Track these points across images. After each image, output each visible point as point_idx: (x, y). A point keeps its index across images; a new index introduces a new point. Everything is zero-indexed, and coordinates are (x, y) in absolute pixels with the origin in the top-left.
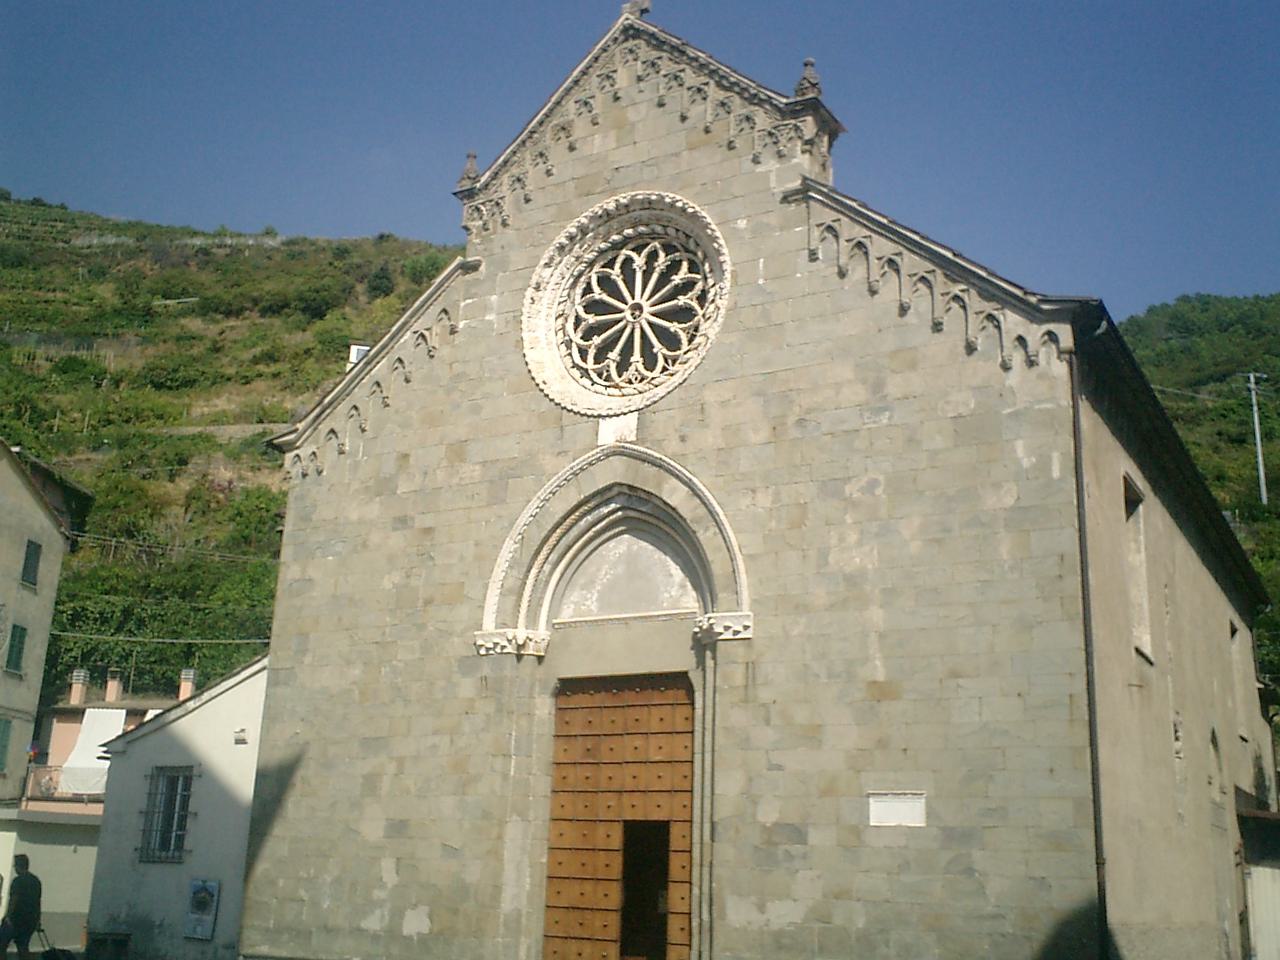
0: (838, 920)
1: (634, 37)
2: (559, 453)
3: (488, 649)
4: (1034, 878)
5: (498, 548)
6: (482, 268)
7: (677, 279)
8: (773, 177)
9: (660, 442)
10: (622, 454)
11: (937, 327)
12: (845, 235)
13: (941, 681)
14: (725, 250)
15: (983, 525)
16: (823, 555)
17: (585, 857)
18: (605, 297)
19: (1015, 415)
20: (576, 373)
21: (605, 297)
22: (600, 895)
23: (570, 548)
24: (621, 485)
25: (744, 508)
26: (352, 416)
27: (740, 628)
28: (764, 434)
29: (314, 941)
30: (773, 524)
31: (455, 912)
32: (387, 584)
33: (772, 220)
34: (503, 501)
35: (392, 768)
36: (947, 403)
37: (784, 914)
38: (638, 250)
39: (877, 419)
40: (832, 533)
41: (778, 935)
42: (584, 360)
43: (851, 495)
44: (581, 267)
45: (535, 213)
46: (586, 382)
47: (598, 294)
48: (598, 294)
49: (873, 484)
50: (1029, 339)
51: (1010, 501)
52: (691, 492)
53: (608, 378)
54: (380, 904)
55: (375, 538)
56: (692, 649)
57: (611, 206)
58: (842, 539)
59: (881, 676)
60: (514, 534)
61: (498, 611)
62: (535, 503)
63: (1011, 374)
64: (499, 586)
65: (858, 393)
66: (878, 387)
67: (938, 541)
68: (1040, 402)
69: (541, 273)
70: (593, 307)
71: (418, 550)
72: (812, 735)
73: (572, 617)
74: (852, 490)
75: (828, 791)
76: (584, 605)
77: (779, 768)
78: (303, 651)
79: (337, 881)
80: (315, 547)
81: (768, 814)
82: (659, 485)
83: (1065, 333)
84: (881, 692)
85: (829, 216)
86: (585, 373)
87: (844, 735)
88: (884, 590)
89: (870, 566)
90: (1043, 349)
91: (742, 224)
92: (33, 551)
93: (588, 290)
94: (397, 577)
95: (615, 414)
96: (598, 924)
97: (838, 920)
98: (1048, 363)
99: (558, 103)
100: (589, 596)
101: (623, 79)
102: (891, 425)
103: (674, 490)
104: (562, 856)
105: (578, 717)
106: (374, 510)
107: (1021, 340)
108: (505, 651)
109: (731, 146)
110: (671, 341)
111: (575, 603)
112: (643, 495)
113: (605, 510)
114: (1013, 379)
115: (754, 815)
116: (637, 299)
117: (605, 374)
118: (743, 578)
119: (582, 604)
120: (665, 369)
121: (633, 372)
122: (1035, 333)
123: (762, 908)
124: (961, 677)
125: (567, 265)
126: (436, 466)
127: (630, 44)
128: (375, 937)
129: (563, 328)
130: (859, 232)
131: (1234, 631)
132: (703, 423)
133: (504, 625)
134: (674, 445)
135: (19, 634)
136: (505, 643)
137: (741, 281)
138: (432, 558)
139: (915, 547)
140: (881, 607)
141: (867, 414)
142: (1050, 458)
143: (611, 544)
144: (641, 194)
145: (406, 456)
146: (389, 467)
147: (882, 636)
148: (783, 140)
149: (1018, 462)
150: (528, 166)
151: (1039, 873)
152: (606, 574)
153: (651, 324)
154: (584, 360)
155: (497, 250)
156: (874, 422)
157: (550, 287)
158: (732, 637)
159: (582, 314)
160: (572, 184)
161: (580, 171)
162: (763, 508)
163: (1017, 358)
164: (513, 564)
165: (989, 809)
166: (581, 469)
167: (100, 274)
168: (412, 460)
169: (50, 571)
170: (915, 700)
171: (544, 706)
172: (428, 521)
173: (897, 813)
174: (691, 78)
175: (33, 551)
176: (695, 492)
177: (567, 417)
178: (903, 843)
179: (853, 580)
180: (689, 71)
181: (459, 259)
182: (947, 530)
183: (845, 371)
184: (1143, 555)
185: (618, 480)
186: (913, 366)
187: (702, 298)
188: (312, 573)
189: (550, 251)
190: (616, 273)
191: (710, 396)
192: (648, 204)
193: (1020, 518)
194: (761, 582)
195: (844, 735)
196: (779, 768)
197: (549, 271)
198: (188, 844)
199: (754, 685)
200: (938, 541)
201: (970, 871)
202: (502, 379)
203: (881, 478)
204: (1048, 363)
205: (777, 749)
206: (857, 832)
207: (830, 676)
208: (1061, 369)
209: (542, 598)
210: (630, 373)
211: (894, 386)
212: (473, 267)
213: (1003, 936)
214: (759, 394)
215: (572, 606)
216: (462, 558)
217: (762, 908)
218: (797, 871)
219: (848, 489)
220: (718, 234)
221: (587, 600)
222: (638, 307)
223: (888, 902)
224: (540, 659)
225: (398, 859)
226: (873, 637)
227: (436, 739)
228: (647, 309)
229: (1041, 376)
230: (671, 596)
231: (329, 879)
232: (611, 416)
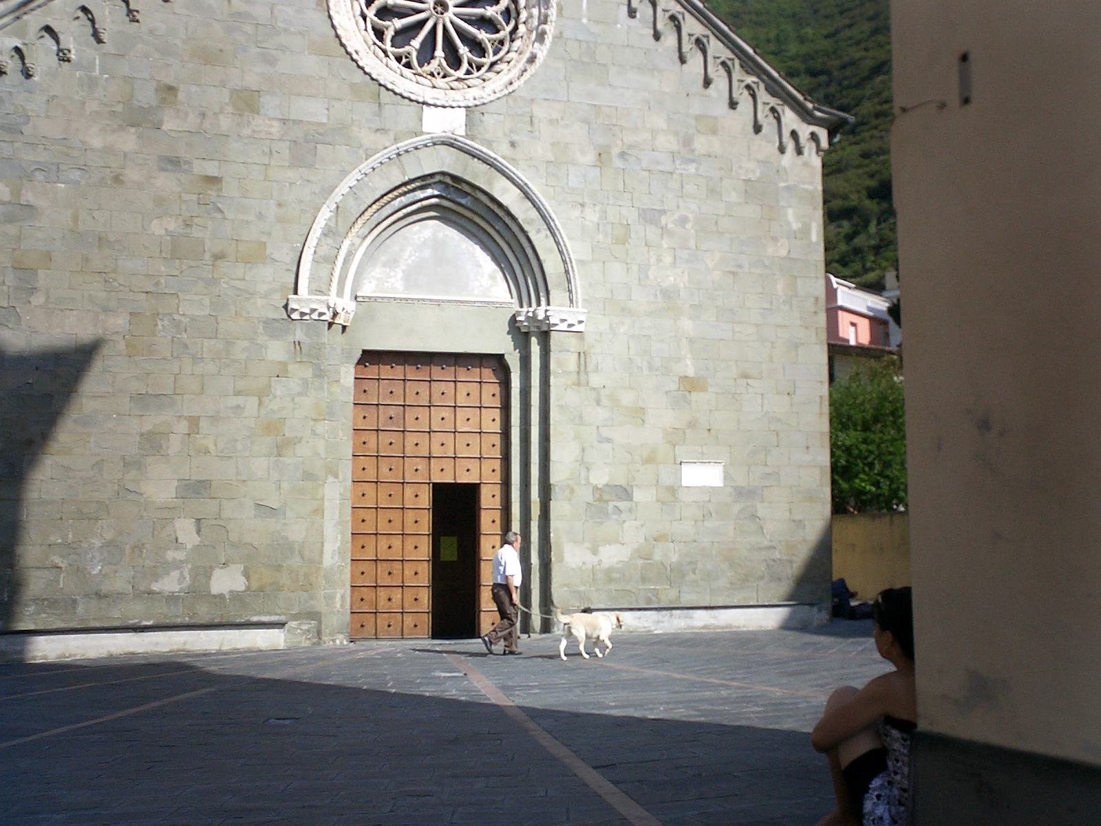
0: (657, 557)
2: (378, 130)
3: (303, 314)
4: (794, 521)
10: (451, 145)
13: (735, 379)
15: (766, 266)
19: (788, 188)
25: (573, 218)
26: (78, 18)
27: (575, 322)
28: (590, 158)
29: (80, 609)
31: (278, 568)
35: (183, 427)
36: (740, 167)
37: (612, 555)
39: (686, 168)
40: (651, 253)
41: (609, 572)
43: (666, 224)
49: (683, 221)
50: (800, 134)
51: (783, 253)
52: (522, 195)
54: (177, 565)
55: (133, 174)
56: (508, 333)
58: (659, 260)
59: (691, 372)
64: (313, 252)
66: (687, 142)
67: (734, 274)
71: (199, 198)
72: (638, 414)
73: (375, 292)
75: (650, 460)
76: (387, 282)
77: (609, 440)
80: (32, 168)
81: (600, 477)
82: (490, 183)
84: (691, 385)
87: (662, 417)
89: (682, 285)
97: (657, 557)
98: (810, 155)
100: (392, 274)
102: (698, 175)
103: (505, 190)
105: (371, 386)
107: (794, 134)
108: (323, 318)
111: (378, 279)
112: (466, 188)
113: (420, 194)
115: (587, 478)
117: (404, 60)
121: (436, 66)
122: (805, 130)
123: (595, 552)
124: (750, 378)
126: (217, 110)
128: (172, 598)
134: (505, 148)
136: (324, 310)
137: (565, 13)
138: (220, 211)
139: (717, 275)
140: (691, 318)
143: (416, 227)
147: (691, 341)
149: (789, 224)
151: (797, 517)
152: (410, 257)
156: (684, 169)
158: (317, 318)
162: (591, 221)
163: (790, 146)
165: (766, 474)
166: (407, 151)
170: (717, 393)
171: (348, 374)
172: (211, 169)
173: (703, 476)
177: (386, 96)
179: (668, 294)
185: (445, 169)
186: (714, 132)
191: (539, 112)
194: (590, 285)
195: (662, 417)
196: (609, 440)
199: (586, 373)
200: (734, 274)
201: (754, 517)
203: (691, 216)
204: (810, 155)
205: (606, 426)
207: (651, 369)
208: (817, 162)
211: (701, 144)
213: (774, 560)
215: (374, 282)
216: (260, 216)
217: (595, 552)
218: (624, 522)
219: (664, 220)
221: (391, 277)
223: (695, 541)
224: (344, 327)
225: (198, 520)
226: (684, 342)
227: (240, 400)
230: (481, 286)
231: (97, 543)
232: (436, 106)
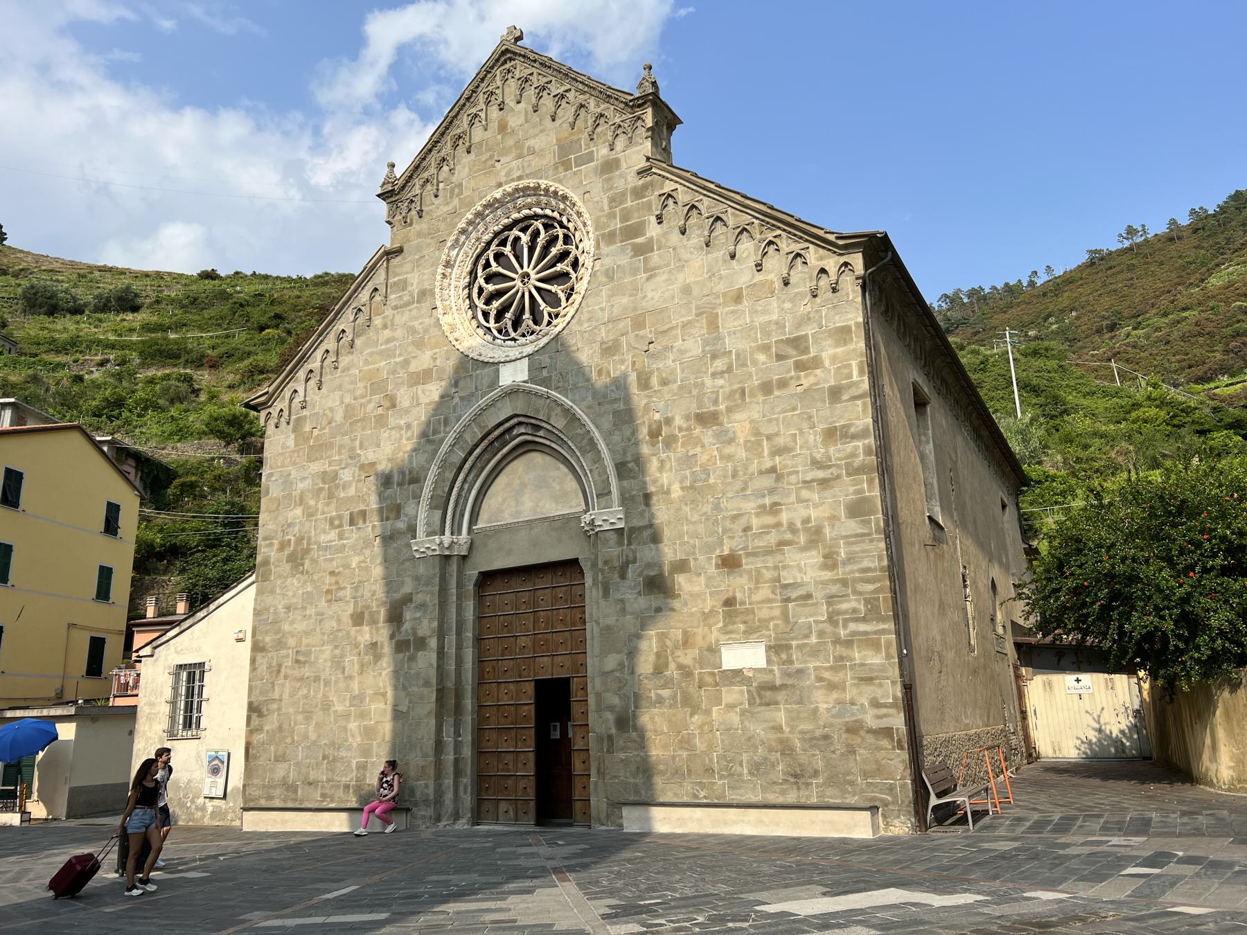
38: (524, 230)
42: (487, 321)
46: (489, 337)
99: (456, 116)
110: (553, 301)
116: (529, 271)
120: (549, 323)
122: (832, 263)
125: (469, 250)
129: (469, 297)
135: (105, 574)
153: (538, 289)
154: (487, 321)
190: (507, 250)
220: (583, 210)
224: (464, 557)
228: (533, 276)
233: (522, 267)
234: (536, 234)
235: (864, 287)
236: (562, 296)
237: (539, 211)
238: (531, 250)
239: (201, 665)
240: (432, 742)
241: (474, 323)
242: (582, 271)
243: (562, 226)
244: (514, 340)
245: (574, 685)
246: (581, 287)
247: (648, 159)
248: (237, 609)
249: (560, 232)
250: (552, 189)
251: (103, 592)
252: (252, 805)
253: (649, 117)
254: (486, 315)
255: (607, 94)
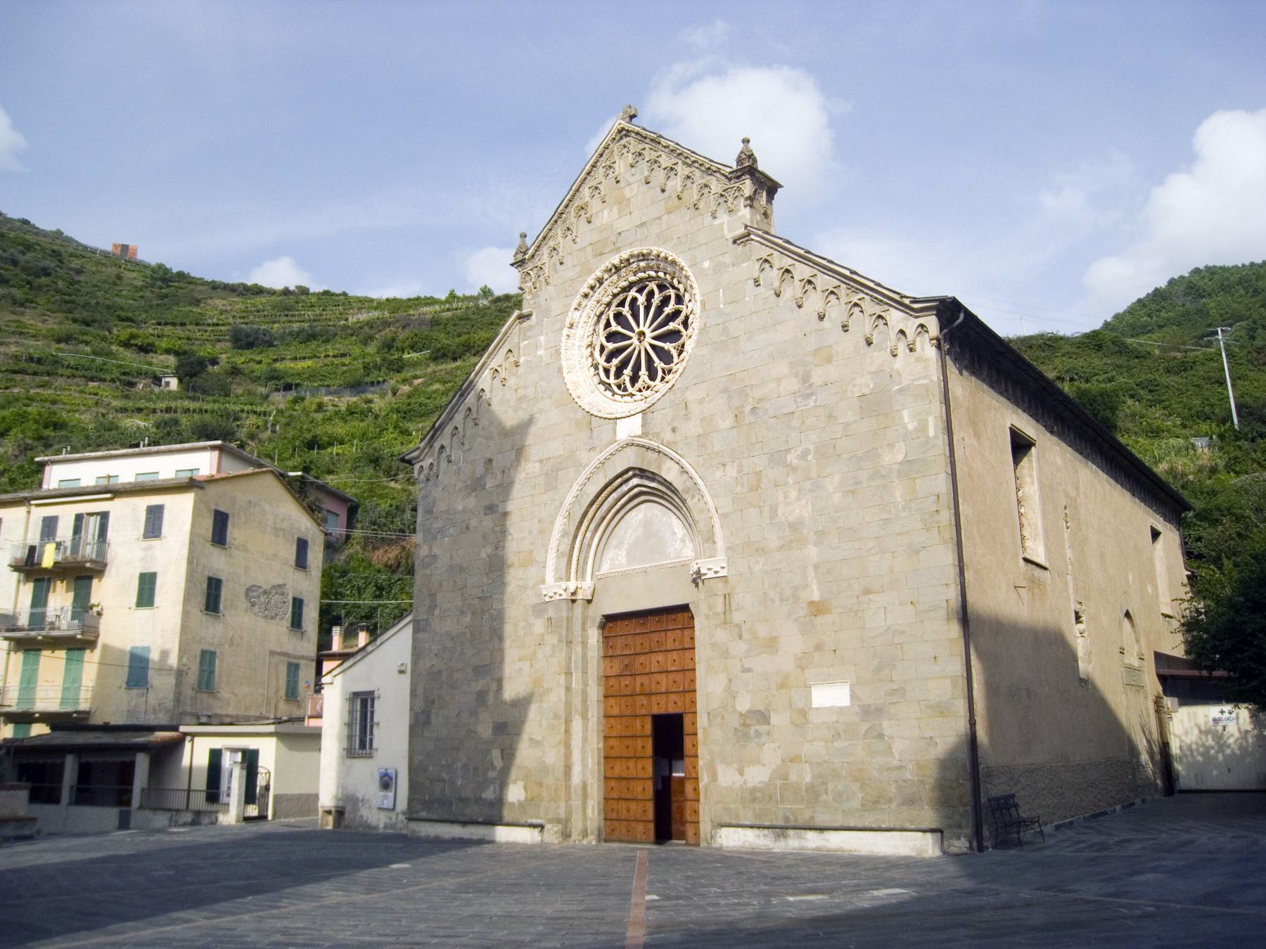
0: (793, 777)
1: (626, 136)
5: (552, 523)
6: (534, 317)
7: (667, 310)
8: (725, 226)
9: (657, 435)
11: (845, 328)
12: (777, 265)
14: (695, 285)
16: (774, 510)
17: (629, 742)
18: (619, 329)
19: (901, 390)
20: (602, 387)
21: (619, 329)
22: (639, 767)
23: (604, 518)
24: (634, 469)
28: (730, 421)
30: (739, 489)
31: (540, 784)
32: (483, 555)
33: (727, 259)
34: (555, 488)
37: (757, 776)
38: (640, 291)
42: (608, 377)
44: (601, 309)
45: (567, 272)
46: (609, 394)
47: (615, 327)
48: (615, 327)
49: (805, 453)
51: (900, 457)
53: (625, 390)
55: (473, 523)
57: (616, 262)
58: (786, 497)
60: (563, 512)
61: (556, 569)
62: (576, 487)
63: (898, 358)
65: (792, 384)
66: (806, 378)
67: (852, 492)
68: (918, 379)
69: (573, 316)
70: (611, 337)
72: (771, 645)
74: (791, 458)
77: (749, 670)
78: (433, 607)
79: (465, 766)
81: (743, 705)
82: (659, 467)
83: (932, 323)
84: (818, 609)
85: (764, 252)
86: (608, 387)
87: (793, 642)
88: (816, 533)
90: (918, 339)
91: (706, 264)
92: (302, 545)
93: (608, 325)
94: (489, 550)
95: (626, 416)
96: (640, 789)
99: (578, 190)
101: (621, 167)
104: (613, 742)
105: (620, 642)
106: (472, 502)
109: (696, 207)
110: (666, 357)
114: (899, 363)
115: (734, 706)
116: (642, 328)
118: (718, 532)
119: (615, 559)
120: (663, 378)
122: (911, 325)
123: (741, 773)
125: (592, 308)
127: (624, 141)
129: (592, 355)
130: (786, 262)
131: (1155, 534)
132: (687, 417)
133: (560, 579)
134: (668, 436)
135: (298, 604)
139: (836, 498)
140: (815, 545)
141: (799, 400)
142: (927, 421)
143: (633, 513)
144: (636, 251)
145: (490, 460)
146: (480, 470)
147: (816, 567)
148: (730, 199)
149: (904, 426)
150: (560, 239)
151: (928, 734)
153: (653, 346)
154: (608, 377)
155: (543, 302)
157: (581, 325)
159: (605, 343)
160: (590, 248)
161: (596, 237)
163: (902, 348)
164: (565, 534)
167: (366, 341)
168: (494, 463)
169: (316, 556)
171: (594, 636)
173: (831, 697)
174: (666, 161)
175: (302, 545)
176: (684, 471)
177: (595, 421)
178: (835, 719)
179: (795, 527)
180: (664, 156)
181: (516, 313)
182: (857, 483)
183: (782, 368)
184: (1036, 486)
185: (631, 465)
186: (829, 360)
187: (685, 324)
188: (435, 551)
189: (578, 299)
190: (626, 311)
191: (691, 396)
192: (644, 257)
193: (909, 468)
196: (749, 670)
197: (578, 313)
198: (375, 745)
200: (852, 492)
201: (881, 736)
202: (550, 397)
203: (811, 447)
204: (923, 349)
206: (803, 714)
207: (782, 600)
208: (931, 353)
209: (586, 558)
210: (639, 385)
211: (817, 377)
212: (528, 316)
214: (725, 390)
216: (530, 532)
217: (741, 773)
220: (690, 274)
222: (642, 334)
224: (589, 601)
226: (811, 568)
228: (649, 334)
229: (918, 360)
231: (460, 765)
233: (638, 325)
234: (651, 294)
235: (939, 347)
236: (674, 353)
237: (653, 274)
238: (647, 308)
239: (372, 693)
240: (562, 768)
241: (596, 379)
242: (690, 329)
243: (674, 287)
244: (632, 395)
245: (687, 720)
246: (689, 347)
247: (746, 226)
248: (398, 644)
249: (672, 292)
250: (662, 255)
251: (297, 622)
252: (415, 816)
253: (748, 186)
254: (607, 371)
255: (710, 170)
